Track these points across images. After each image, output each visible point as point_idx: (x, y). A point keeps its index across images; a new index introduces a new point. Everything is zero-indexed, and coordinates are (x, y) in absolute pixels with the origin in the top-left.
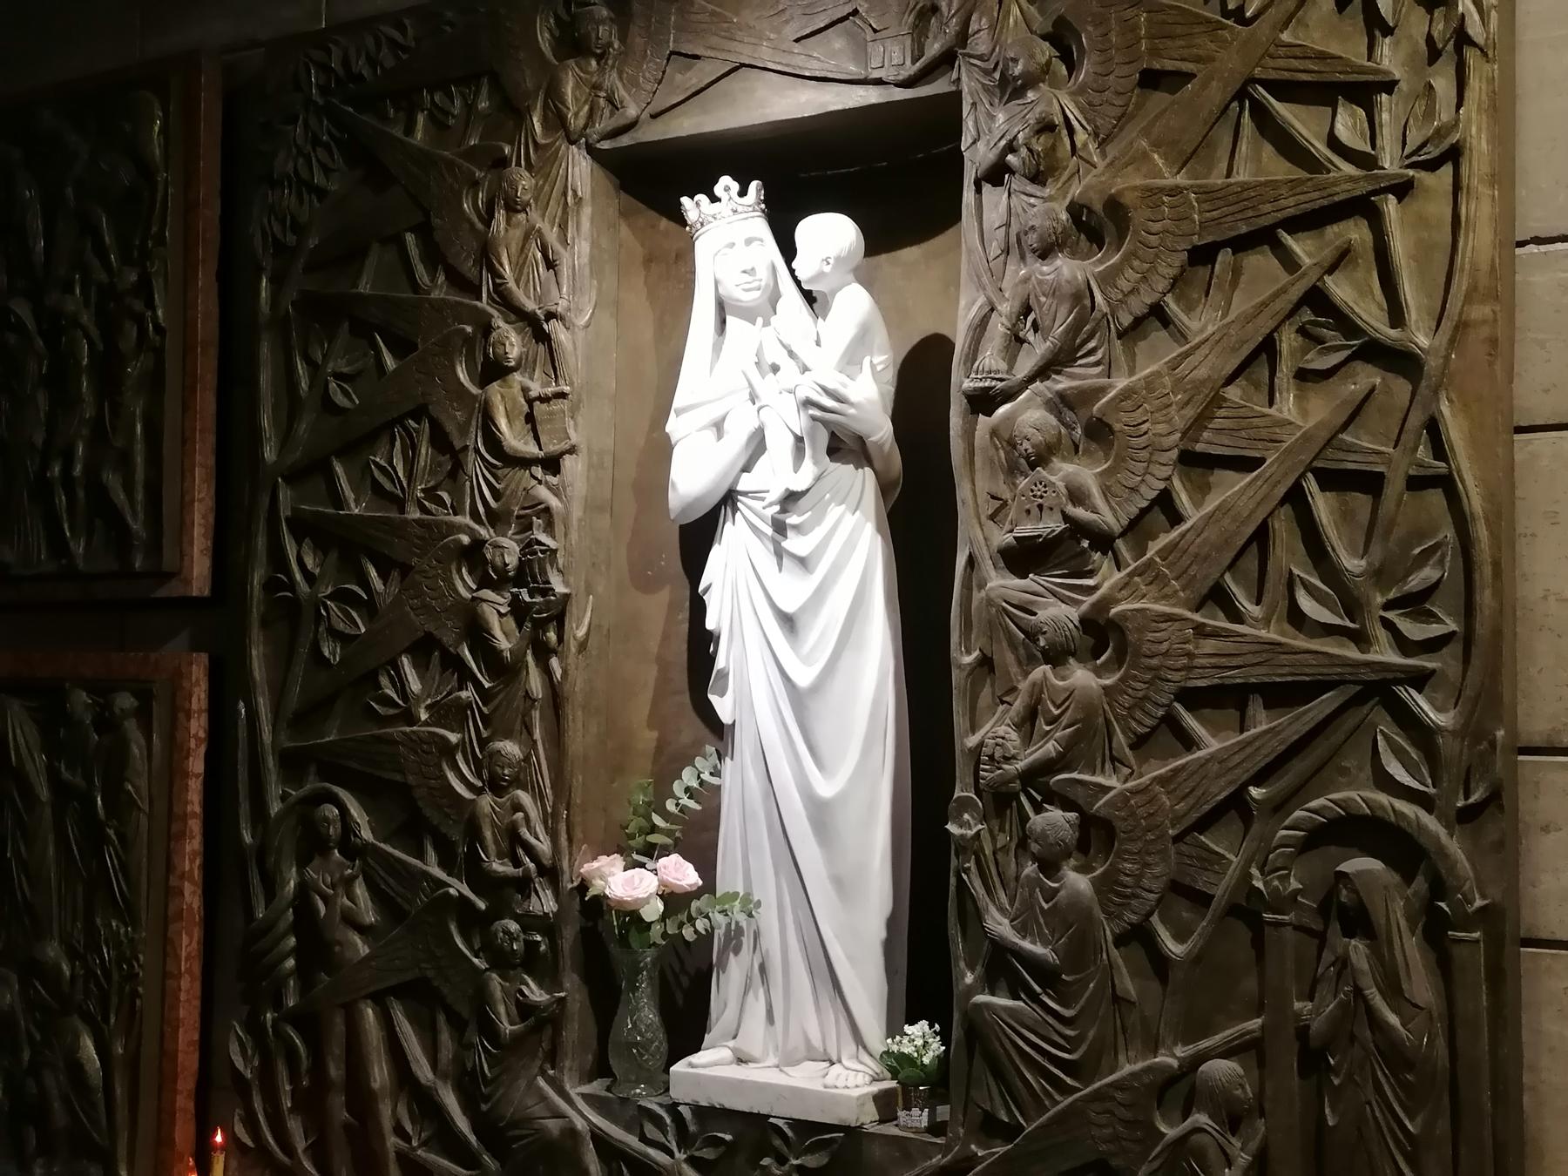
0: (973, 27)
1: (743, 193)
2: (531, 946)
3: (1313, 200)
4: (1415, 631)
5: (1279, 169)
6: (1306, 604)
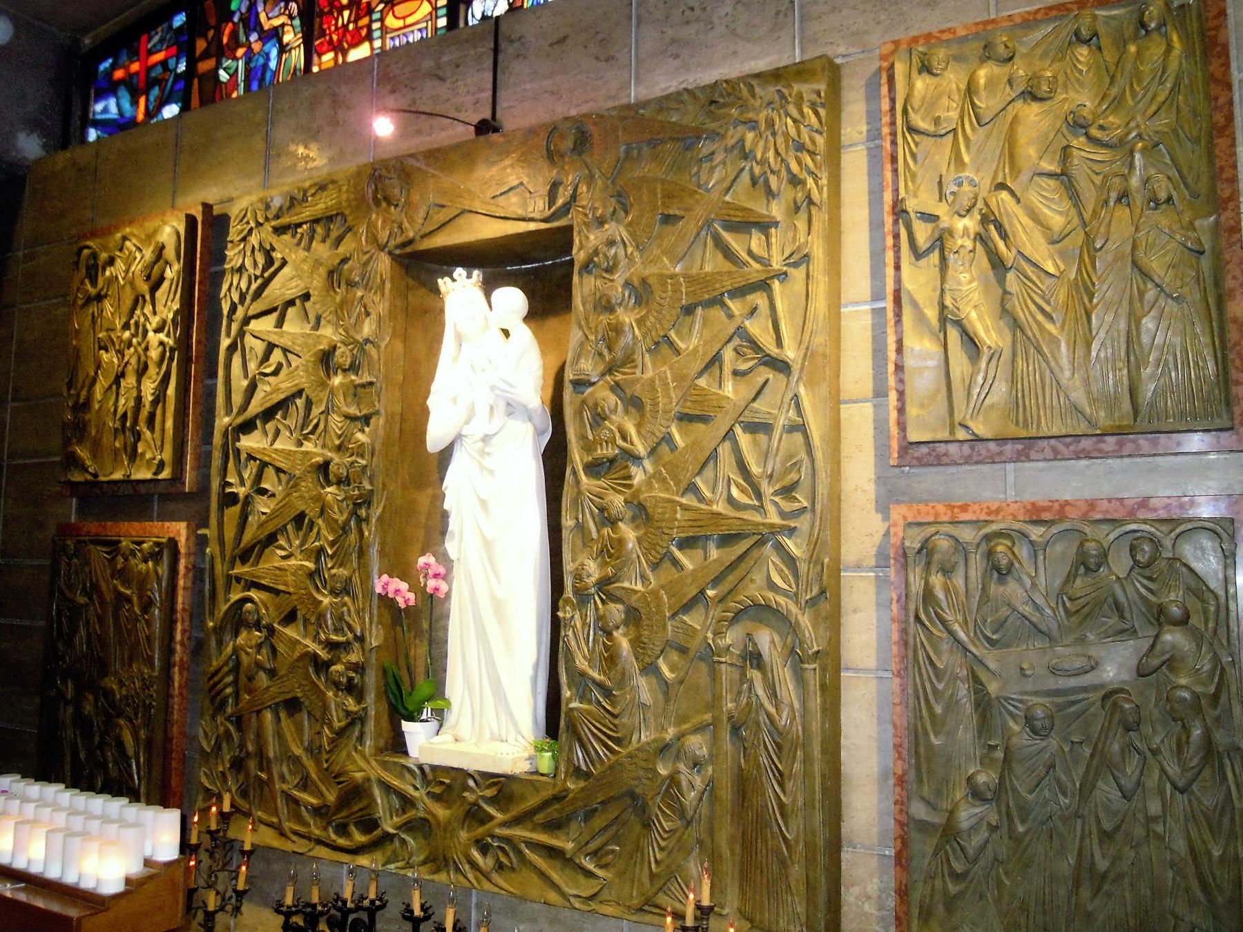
0: (579, 191)
1: (469, 276)
2: (350, 679)
3: (739, 282)
4: (787, 506)
5: (726, 266)
6: (735, 492)
